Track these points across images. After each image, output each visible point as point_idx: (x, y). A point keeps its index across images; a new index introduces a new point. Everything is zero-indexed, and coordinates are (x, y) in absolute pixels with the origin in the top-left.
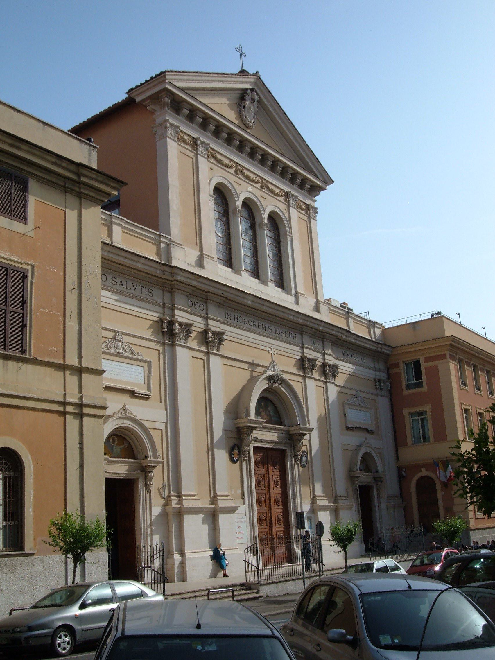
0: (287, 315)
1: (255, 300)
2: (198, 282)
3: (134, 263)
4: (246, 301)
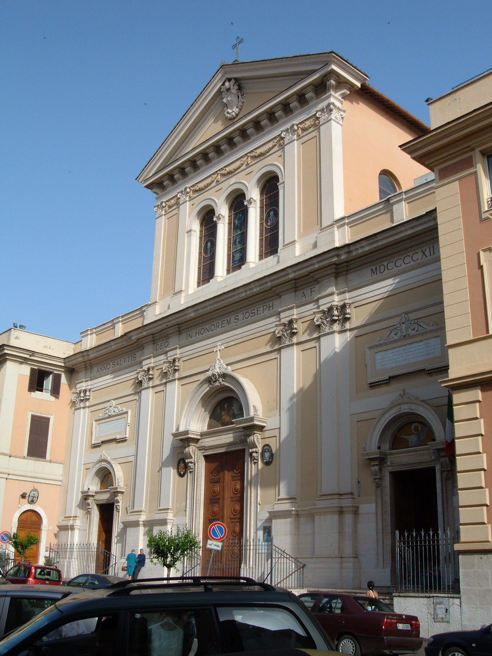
0: (237, 297)
1: (195, 309)
2: (147, 330)
3: (110, 349)
4: (188, 316)
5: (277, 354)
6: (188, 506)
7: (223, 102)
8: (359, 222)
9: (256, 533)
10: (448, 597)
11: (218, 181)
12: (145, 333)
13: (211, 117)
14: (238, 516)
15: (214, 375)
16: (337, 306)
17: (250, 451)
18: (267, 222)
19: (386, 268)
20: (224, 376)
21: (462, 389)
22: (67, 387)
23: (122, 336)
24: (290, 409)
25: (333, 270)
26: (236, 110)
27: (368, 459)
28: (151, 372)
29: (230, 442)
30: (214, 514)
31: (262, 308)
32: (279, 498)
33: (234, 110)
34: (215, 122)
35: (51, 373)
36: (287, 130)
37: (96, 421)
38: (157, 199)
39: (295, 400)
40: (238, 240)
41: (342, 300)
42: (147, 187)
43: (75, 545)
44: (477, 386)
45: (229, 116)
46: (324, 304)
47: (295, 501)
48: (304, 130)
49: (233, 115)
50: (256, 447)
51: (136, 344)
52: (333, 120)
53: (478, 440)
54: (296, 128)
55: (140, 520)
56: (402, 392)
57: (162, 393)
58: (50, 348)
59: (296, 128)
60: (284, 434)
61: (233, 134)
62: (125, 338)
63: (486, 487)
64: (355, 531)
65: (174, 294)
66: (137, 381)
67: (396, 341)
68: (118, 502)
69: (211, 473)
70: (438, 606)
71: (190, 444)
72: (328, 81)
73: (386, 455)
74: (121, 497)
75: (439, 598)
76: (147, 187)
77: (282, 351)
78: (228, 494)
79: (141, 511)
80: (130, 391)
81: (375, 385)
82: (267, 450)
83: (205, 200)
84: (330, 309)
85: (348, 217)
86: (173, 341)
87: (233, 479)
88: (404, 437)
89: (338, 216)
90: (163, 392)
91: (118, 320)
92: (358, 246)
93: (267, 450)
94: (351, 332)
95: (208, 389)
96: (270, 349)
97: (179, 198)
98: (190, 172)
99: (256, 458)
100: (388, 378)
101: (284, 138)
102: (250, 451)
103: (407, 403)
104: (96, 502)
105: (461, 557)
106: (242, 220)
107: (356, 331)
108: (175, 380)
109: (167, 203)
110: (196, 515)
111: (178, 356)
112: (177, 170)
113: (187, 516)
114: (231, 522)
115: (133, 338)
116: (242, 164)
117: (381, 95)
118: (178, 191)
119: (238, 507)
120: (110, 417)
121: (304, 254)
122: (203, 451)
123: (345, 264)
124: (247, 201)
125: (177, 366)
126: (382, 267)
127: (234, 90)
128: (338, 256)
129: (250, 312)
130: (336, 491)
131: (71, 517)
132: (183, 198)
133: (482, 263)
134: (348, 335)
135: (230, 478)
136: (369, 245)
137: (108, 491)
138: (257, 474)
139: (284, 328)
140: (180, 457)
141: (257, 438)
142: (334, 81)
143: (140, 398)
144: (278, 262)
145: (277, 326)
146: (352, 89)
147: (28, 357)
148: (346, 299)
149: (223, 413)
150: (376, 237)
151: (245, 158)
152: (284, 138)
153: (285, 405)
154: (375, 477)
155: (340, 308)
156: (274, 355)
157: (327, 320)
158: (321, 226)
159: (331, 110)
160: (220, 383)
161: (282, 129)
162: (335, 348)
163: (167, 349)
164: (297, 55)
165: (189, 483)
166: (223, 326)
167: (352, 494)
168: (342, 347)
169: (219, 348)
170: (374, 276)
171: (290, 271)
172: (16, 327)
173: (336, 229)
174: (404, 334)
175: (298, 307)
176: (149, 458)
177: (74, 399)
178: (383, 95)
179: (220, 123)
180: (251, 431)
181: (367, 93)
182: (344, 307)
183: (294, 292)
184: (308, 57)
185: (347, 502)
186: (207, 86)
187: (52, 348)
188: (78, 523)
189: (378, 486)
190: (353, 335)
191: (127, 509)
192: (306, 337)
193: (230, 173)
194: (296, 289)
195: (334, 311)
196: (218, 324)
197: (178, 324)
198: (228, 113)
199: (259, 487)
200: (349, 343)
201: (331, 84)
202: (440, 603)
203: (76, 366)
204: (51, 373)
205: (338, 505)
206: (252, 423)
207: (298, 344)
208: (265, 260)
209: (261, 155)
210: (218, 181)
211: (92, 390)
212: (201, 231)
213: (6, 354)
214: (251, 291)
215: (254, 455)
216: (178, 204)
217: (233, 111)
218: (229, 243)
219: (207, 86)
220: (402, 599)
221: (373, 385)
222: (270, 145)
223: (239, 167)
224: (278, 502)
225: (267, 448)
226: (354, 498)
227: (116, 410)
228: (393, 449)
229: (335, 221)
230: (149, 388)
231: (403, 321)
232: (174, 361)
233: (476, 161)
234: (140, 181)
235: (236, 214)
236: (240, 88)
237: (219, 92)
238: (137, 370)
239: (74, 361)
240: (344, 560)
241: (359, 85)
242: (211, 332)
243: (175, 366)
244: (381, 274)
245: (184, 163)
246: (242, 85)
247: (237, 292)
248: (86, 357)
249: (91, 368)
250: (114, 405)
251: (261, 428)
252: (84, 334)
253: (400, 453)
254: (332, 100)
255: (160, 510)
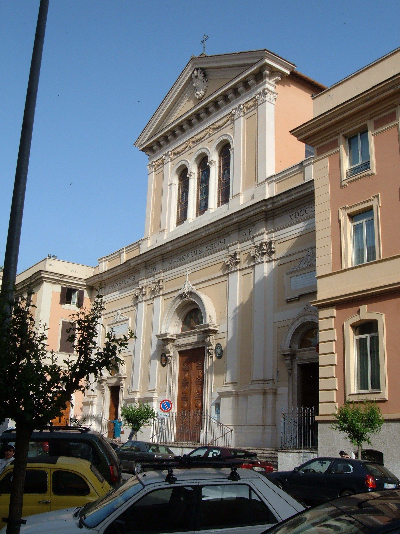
0: (200, 235)
1: (172, 243)
4: (168, 249)
5: (252, 269)
6: (167, 388)
7: (193, 86)
8: (282, 180)
9: (211, 407)
10: (311, 452)
11: (190, 147)
12: (139, 261)
13: (186, 97)
14: (200, 396)
15: (184, 293)
16: (266, 242)
17: (208, 348)
18: (223, 178)
19: (299, 214)
20: (191, 293)
21: (322, 308)
22: (89, 300)
23: (124, 263)
24: (234, 318)
25: (264, 216)
26: (202, 92)
27: (284, 355)
28: (144, 290)
29: (195, 342)
30: (185, 394)
31: (217, 243)
32: (226, 382)
33: (201, 92)
34: (189, 101)
35: (77, 290)
36: (236, 109)
37: (108, 325)
38: (149, 159)
39: (237, 311)
40: (203, 192)
41: (269, 238)
42: (142, 150)
43: (95, 415)
44: (334, 306)
45: (197, 97)
46: (258, 241)
47: (236, 385)
48: (248, 108)
49: (200, 96)
50: (211, 345)
51: (134, 269)
52: (267, 101)
53: (332, 344)
54: (242, 107)
55: (135, 398)
56: (306, 307)
57: (151, 305)
58: (75, 272)
59: (242, 107)
60: (230, 336)
61: (200, 111)
62: (126, 264)
63: (336, 377)
64: (274, 407)
65: (257, 185)
66: (135, 296)
67: (303, 269)
68: (122, 385)
69: (183, 364)
70: (305, 458)
71: (169, 343)
72: (264, 71)
73: (296, 352)
74: (124, 381)
75: (305, 453)
76: (142, 150)
77: (256, 267)
78: (194, 379)
79: (154, 390)
80: (131, 304)
81: (290, 301)
82: (218, 348)
83: (181, 161)
84: (261, 245)
85: (276, 176)
86: (159, 266)
87: (198, 368)
88: (308, 339)
89: (268, 175)
90: (152, 304)
91: (310, 162)
92: (279, 198)
93: (218, 348)
94: (276, 262)
95: (180, 303)
96: (222, 274)
97: (164, 159)
98: (187, 129)
99: (211, 353)
100: (298, 296)
101: (234, 114)
102: (208, 348)
103: (309, 314)
104: (108, 385)
105: (319, 425)
106: (207, 176)
107: (278, 261)
108: (159, 296)
109: (156, 162)
110: (172, 394)
111: (162, 278)
112: (162, 137)
113: (167, 395)
114: (196, 400)
115: (132, 265)
116: (206, 134)
117: (308, 79)
118: (163, 154)
119: (200, 389)
120: (117, 322)
121: (245, 203)
122: (178, 348)
123: (272, 211)
124: (209, 162)
125: (161, 286)
126: (297, 213)
127: (201, 78)
128: (266, 205)
129: (209, 246)
130: (261, 377)
131: (91, 396)
132: (167, 159)
133: (341, 218)
134: (274, 264)
135: (196, 368)
136: (287, 197)
137: (115, 377)
138: (212, 365)
139: (231, 259)
140: (163, 352)
141: (212, 339)
142: (268, 71)
143: (137, 308)
144: (228, 209)
145: (226, 256)
146: (283, 76)
147: (59, 279)
148: (272, 237)
149: (191, 320)
150: (291, 192)
151: (208, 129)
152: (234, 114)
153: (231, 315)
154: (288, 368)
155: (268, 244)
156: (224, 278)
157: (259, 253)
158: (257, 182)
159: (266, 94)
160: (188, 298)
161: (233, 108)
162: (264, 274)
163: (155, 273)
164: (242, 52)
165: (168, 371)
166: (215, 247)
167: (273, 380)
168: (269, 273)
169: (188, 272)
170: (292, 220)
171: (234, 216)
172: (50, 257)
173: (267, 184)
174: (309, 264)
175: (241, 243)
176: (142, 353)
177: (252, 254)
178: (309, 78)
179: (192, 102)
180: (208, 334)
181: (297, 77)
182: (270, 243)
183: (238, 232)
184: (249, 53)
185: (269, 386)
186: (182, 74)
187: (77, 271)
188: (96, 400)
189: (290, 374)
190: (277, 264)
191: (128, 390)
192: (245, 265)
193: (198, 140)
194: (239, 229)
195: (264, 246)
196: (188, 255)
197: (162, 255)
198: (197, 94)
199: (213, 374)
200: (274, 270)
201: (265, 74)
202: (306, 457)
203: (95, 284)
204: (77, 290)
205: (262, 388)
206: (208, 328)
207: (241, 270)
208: (221, 207)
209: (219, 127)
210: (190, 147)
211: (105, 303)
212: (179, 184)
213: (42, 277)
214: (209, 231)
215: (210, 351)
216: (163, 164)
217: (200, 93)
218: (198, 194)
219: (182, 74)
220: (283, 453)
221: (289, 301)
222: (225, 120)
223: (185, 149)
224: (225, 385)
225: (218, 346)
226: (274, 383)
227: (121, 318)
228: (301, 348)
229: (266, 179)
230: (142, 301)
231: (309, 254)
232: (159, 281)
233: (398, 115)
234: (137, 146)
235: (202, 172)
236: (205, 76)
237: (191, 79)
238: (134, 288)
239: (93, 281)
240: (266, 427)
241: (288, 72)
242: (184, 261)
243: (237, 259)
244: (296, 219)
245: (182, 122)
246: (207, 73)
247: (199, 232)
248: (101, 278)
249: (105, 286)
250: (120, 314)
251: (215, 332)
252: (100, 260)
253: (305, 351)
254: (267, 86)
255: (149, 391)
